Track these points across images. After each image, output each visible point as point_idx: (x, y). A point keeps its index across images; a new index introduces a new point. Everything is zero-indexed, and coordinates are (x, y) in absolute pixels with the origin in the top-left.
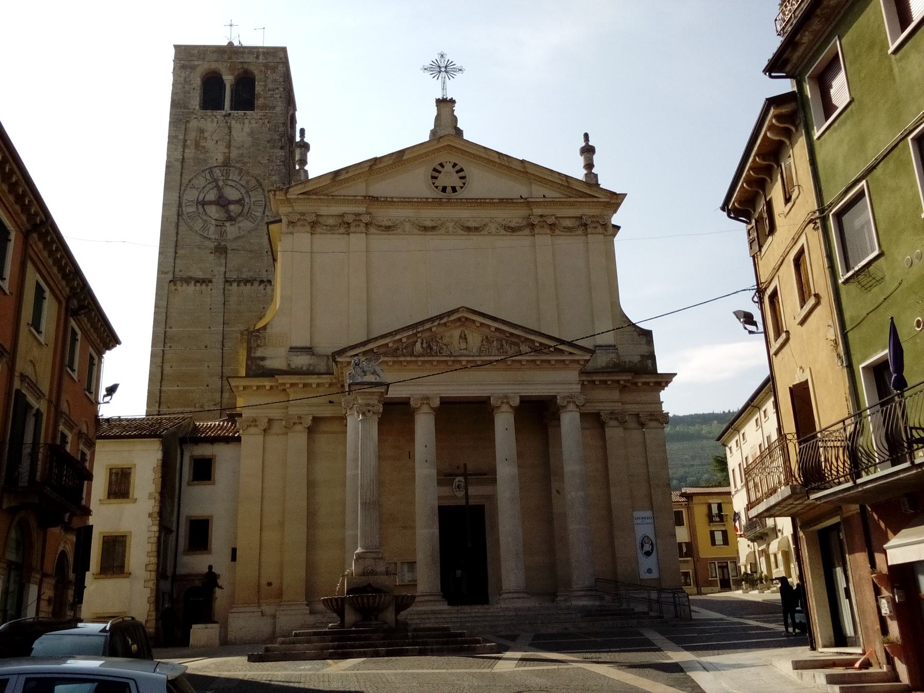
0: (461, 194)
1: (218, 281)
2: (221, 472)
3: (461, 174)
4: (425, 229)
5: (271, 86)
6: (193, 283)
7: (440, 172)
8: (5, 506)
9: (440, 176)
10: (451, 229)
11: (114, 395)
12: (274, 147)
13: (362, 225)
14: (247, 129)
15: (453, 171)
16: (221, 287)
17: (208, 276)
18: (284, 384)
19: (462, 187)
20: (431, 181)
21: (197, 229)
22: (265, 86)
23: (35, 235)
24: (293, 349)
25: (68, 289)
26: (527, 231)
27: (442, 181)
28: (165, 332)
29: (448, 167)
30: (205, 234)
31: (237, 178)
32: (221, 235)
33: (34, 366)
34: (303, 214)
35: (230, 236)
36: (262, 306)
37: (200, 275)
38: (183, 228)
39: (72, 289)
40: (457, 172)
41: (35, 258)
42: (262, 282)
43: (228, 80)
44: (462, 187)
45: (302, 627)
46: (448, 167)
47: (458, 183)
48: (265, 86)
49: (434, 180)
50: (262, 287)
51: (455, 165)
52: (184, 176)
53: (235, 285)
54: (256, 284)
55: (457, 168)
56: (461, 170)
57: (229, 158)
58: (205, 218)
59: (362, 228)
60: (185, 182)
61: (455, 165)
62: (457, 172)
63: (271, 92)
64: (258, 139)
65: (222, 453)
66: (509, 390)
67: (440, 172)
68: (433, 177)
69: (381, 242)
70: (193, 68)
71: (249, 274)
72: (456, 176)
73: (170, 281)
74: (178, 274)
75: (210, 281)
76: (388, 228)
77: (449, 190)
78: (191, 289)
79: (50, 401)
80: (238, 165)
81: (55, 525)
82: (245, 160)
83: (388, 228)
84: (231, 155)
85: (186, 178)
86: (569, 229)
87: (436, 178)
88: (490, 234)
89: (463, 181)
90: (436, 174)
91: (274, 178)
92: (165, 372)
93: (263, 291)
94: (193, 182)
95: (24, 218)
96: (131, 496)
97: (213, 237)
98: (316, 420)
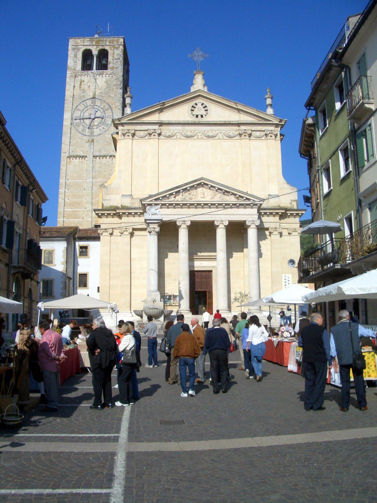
0: (205, 120)
1: (90, 157)
2: (91, 251)
3: (206, 109)
4: (188, 137)
5: (116, 57)
6: (78, 158)
7: (195, 108)
8: (12, 273)
9: (195, 110)
10: (200, 137)
11: (47, 222)
12: (117, 88)
13: (156, 135)
14: (104, 79)
15: (202, 107)
16: (91, 160)
17: (86, 155)
18: (119, 213)
19: (206, 115)
20: (190, 112)
21: (80, 131)
22: (113, 57)
23: (17, 166)
24: (123, 196)
25: (28, 182)
26: (238, 137)
27: (196, 112)
28: (66, 182)
29: (199, 105)
30: (84, 133)
31: (99, 104)
32: (91, 134)
33: (18, 216)
34: (128, 130)
35: (95, 134)
36: (111, 169)
37: (81, 154)
38: (73, 130)
39: (30, 182)
40: (204, 108)
41: (18, 174)
42: (111, 156)
43: (95, 52)
44: (206, 115)
45: (294, 354)
46: (199, 105)
47: (203, 112)
48: (113, 57)
49: (192, 112)
50: (111, 159)
51: (202, 104)
52: (74, 104)
53: (98, 158)
54: (108, 157)
55: (204, 106)
56: (206, 107)
57: (95, 94)
58: (84, 125)
59: (157, 136)
60: (74, 107)
61: (202, 104)
62: (204, 108)
63: (116, 60)
64: (109, 84)
65: (92, 245)
66: (224, 218)
67: (195, 108)
68: (192, 110)
69: (165, 143)
70: (79, 49)
71: (105, 153)
72: (203, 110)
73: (68, 157)
74: (71, 154)
75: (86, 157)
76: (169, 137)
77: (199, 116)
78: (77, 160)
79: (23, 229)
80: (100, 98)
81: (28, 278)
82: (103, 95)
83: (169, 137)
84: (96, 93)
85: (75, 105)
86: (259, 138)
87: (193, 110)
88: (219, 139)
89: (207, 112)
90: (193, 109)
91: (117, 104)
92: (66, 202)
93: (111, 161)
94: (79, 107)
95: (13, 160)
96: (53, 263)
97: (88, 134)
98: (134, 229)
